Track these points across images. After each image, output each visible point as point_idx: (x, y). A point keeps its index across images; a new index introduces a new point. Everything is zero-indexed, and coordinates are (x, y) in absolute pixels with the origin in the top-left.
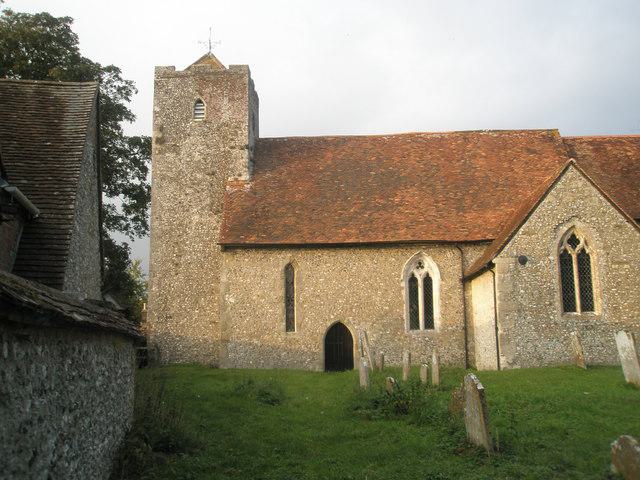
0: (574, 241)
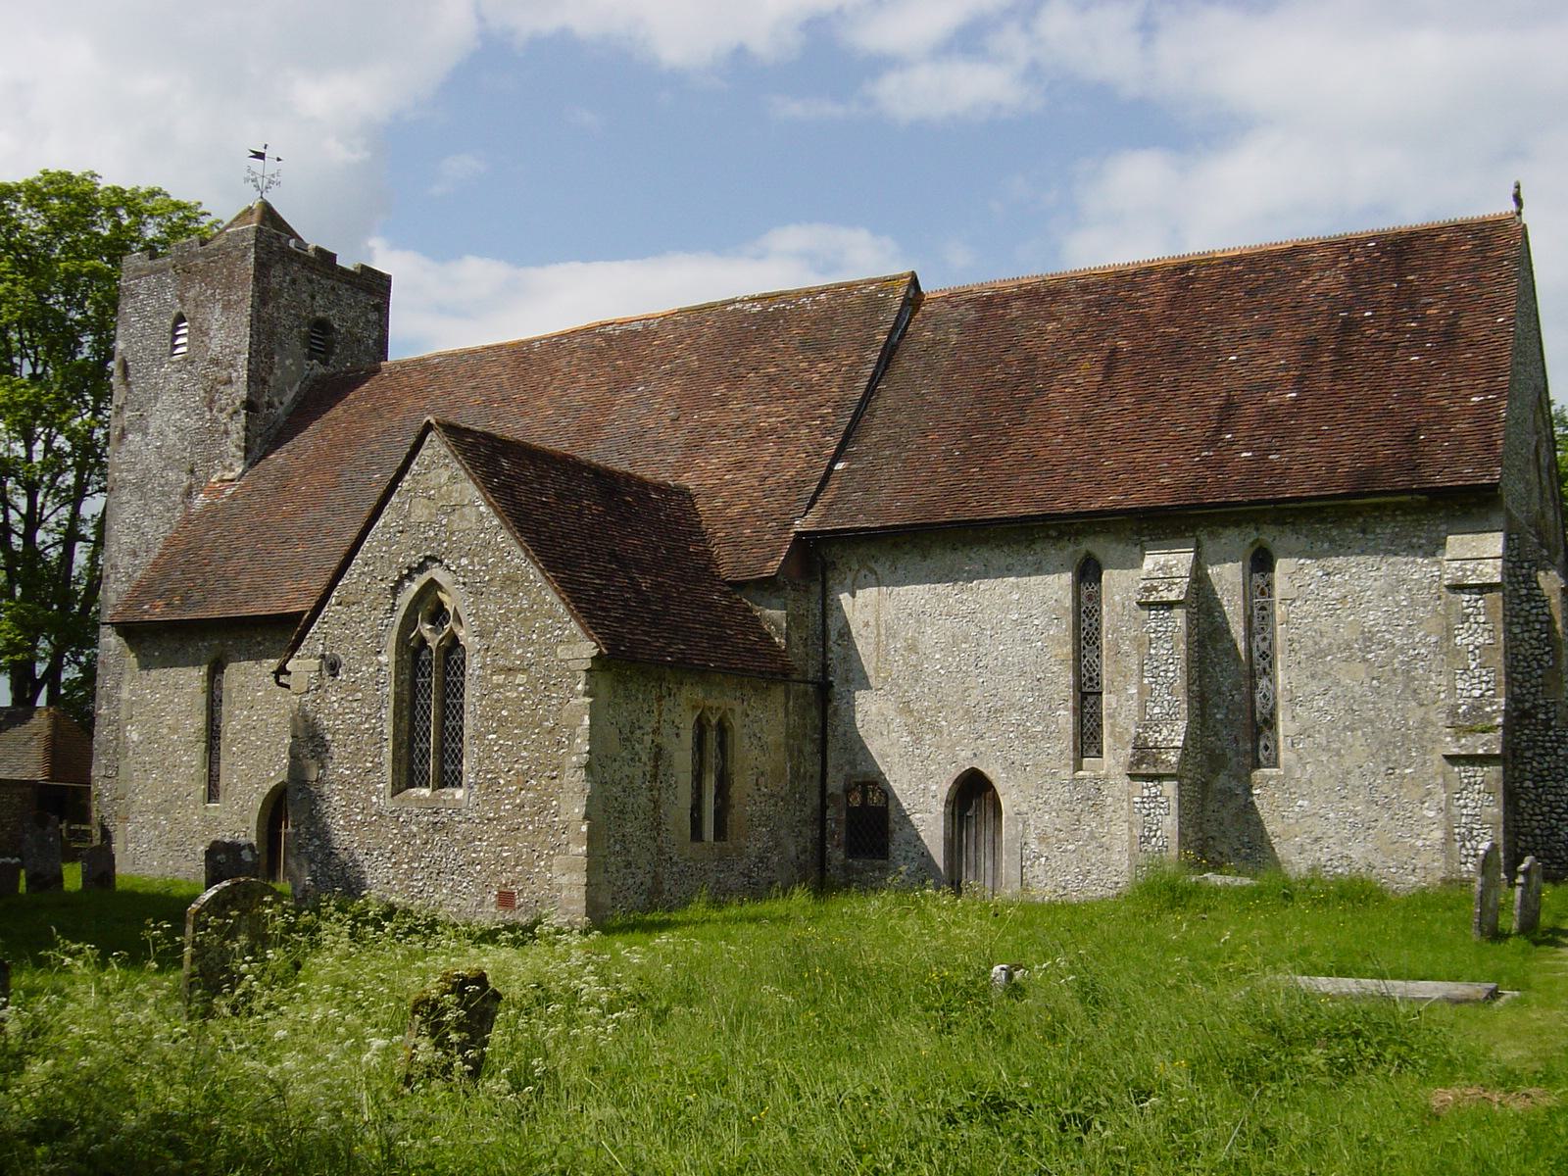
0: (438, 615)
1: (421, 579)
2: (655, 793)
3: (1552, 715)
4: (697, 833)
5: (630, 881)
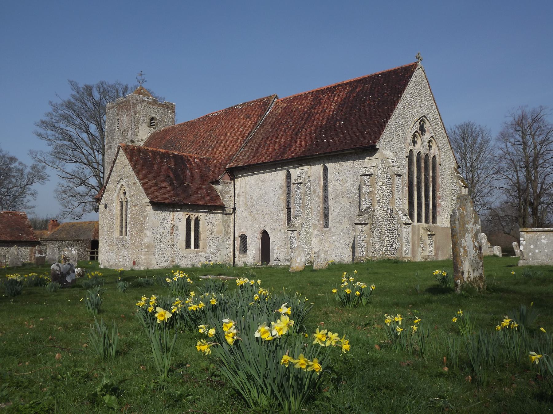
1: (120, 184)
2: (172, 236)
3: (392, 212)
4: (188, 246)
5: (163, 258)
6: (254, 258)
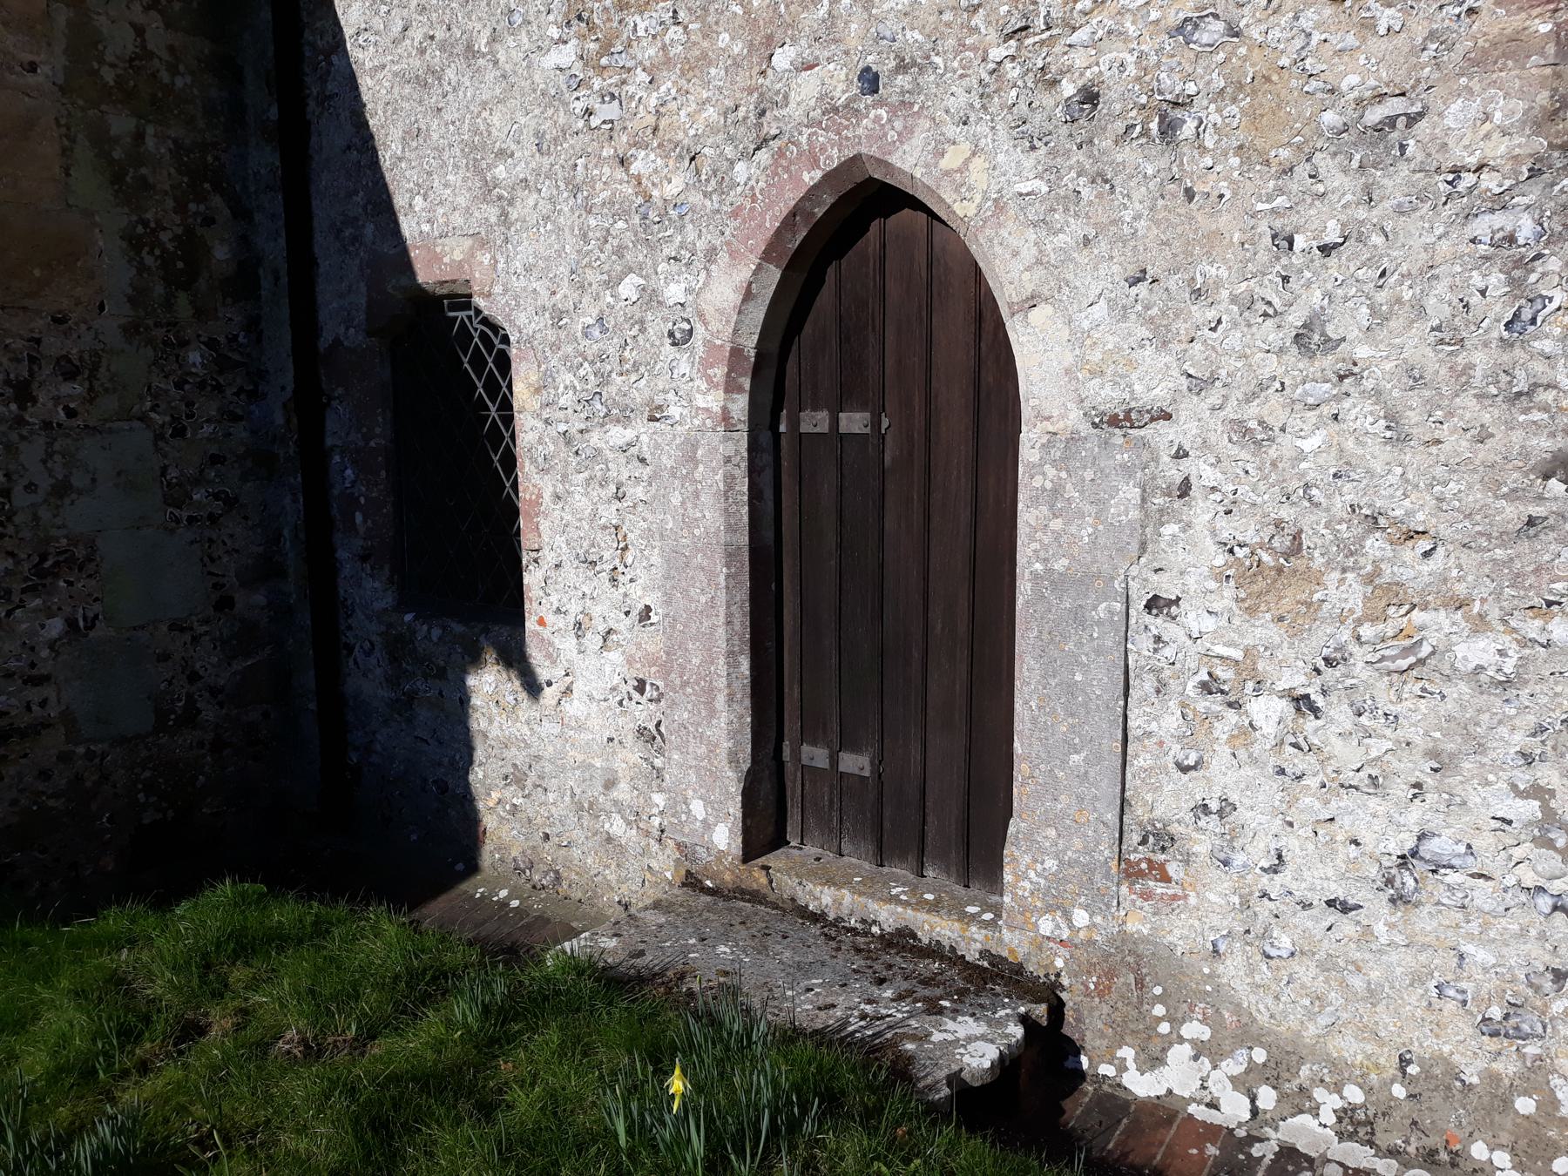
6: (643, 712)
